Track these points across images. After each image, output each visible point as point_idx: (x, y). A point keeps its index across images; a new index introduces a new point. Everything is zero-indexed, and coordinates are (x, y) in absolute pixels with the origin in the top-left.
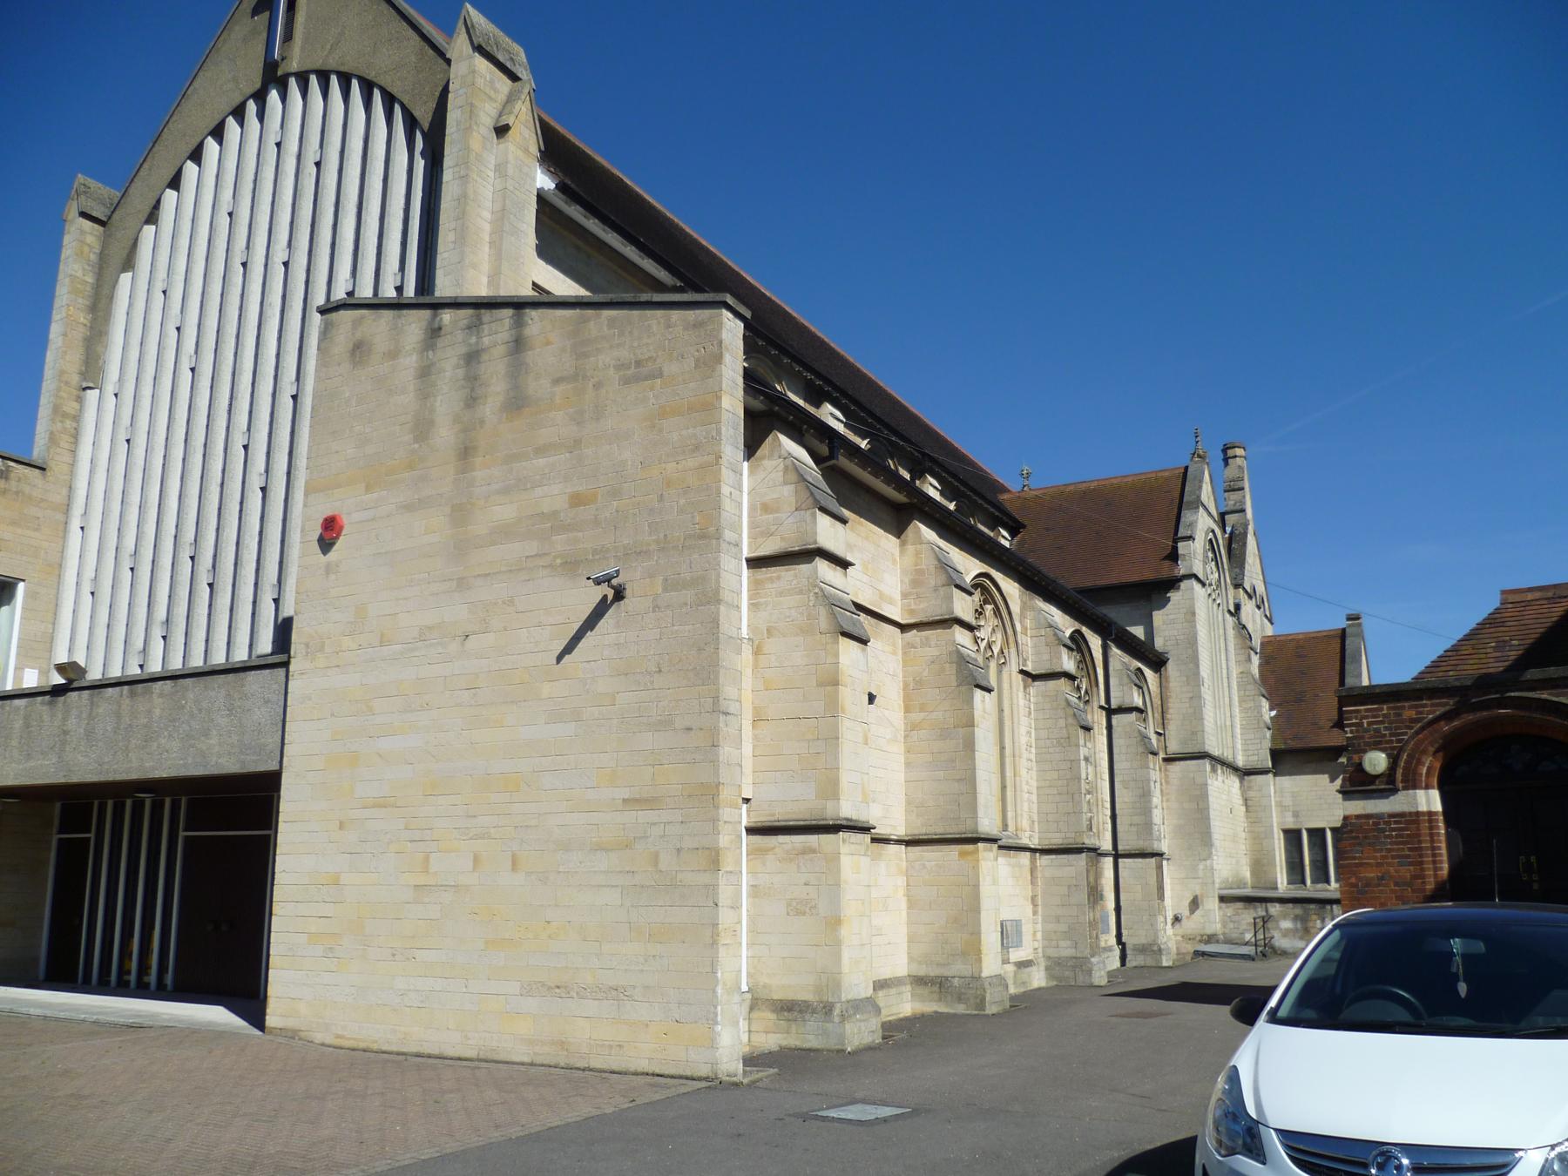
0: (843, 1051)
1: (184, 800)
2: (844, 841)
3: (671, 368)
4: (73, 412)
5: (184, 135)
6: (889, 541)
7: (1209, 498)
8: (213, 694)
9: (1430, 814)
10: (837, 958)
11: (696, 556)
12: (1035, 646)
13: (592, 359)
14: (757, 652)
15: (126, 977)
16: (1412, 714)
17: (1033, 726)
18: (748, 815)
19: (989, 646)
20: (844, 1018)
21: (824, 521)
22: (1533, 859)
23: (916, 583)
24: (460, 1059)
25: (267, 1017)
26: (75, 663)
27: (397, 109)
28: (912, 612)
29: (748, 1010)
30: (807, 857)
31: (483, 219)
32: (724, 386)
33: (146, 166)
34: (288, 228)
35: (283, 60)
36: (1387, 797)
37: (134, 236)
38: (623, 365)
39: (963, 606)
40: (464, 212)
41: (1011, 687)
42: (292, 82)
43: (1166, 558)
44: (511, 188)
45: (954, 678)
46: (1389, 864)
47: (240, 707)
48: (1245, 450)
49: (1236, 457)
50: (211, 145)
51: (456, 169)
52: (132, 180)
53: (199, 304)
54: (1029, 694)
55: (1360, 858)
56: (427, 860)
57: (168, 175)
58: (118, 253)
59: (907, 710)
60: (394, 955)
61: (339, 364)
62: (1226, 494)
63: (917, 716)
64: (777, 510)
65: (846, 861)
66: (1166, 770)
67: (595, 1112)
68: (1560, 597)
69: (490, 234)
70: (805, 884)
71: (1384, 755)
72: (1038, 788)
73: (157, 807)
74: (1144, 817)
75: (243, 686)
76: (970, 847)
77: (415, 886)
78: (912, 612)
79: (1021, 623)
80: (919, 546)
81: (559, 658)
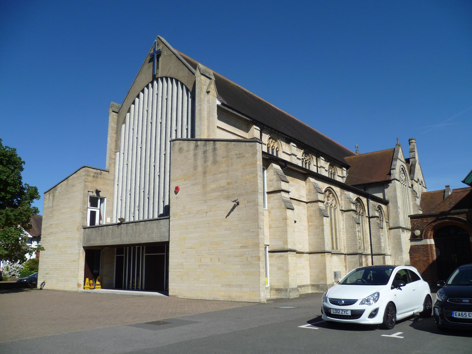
0: (289, 299)
1: (145, 247)
2: (289, 254)
3: (247, 155)
4: (114, 158)
5: (135, 92)
6: (302, 183)
7: (401, 157)
8: (153, 225)
9: (431, 245)
10: (288, 279)
11: (253, 196)
12: (345, 203)
13: (230, 153)
14: (269, 213)
15: (133, 288)
16: (426, 221)
17: (345, 223)
18: (269, 249)
19: (331, 205)
20: (290, 292)
21: (283, 183)
22: (456, 255)
23: (309, 192)
24: (209, 300)
25: (169, 293)
26: (123, 218)
27: (184, 86)
28: (308, 199)
29: (270, 290)
30: (281, 257)
31: (205, 114)
32: (258, 159)
33: (126, 99)
34: (160, 114)
35: (157, 74)
36: (420, 241)
37: (125, 116)
38: (237, 154)
39: (321, 197)
40: (201, 113)
41: (338, 214)
42: (159, 79)
43: (388, 174)
44: (211, 106)
45: (319, 214)
46: (421, 257)
47: (159, 227)
48: (415, 140)
49: (412, 142)
50: (141, 94)
51: (198, 103)
52: (124, 102)
53: (141, 132)
54: (343, 215)
55: (414, 255)
56: (201, 259)
57: (132, 101)
58: (121, 121)
59: (308, 222)
60: (195, 279)
61: (176, 153)
62: (410, 153)
63: (311, 224)
64: (273, 181)
65: (290, 258)
66: (389, 232)
67: (236, 307)
68: (466, 191)
69: (207, 117)
70: (281, 263)
71: (419, 231)
72: (346, 239)
73: (139, 248)
74: (379, 245)
75: (160, 223)
76: (323, 254)
77: (199, 265)
78: (308, 199)
79: (340, 198)
80: (310, 183)
81: (226, 217)
